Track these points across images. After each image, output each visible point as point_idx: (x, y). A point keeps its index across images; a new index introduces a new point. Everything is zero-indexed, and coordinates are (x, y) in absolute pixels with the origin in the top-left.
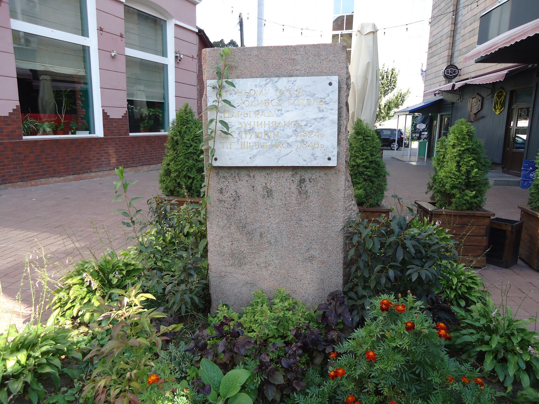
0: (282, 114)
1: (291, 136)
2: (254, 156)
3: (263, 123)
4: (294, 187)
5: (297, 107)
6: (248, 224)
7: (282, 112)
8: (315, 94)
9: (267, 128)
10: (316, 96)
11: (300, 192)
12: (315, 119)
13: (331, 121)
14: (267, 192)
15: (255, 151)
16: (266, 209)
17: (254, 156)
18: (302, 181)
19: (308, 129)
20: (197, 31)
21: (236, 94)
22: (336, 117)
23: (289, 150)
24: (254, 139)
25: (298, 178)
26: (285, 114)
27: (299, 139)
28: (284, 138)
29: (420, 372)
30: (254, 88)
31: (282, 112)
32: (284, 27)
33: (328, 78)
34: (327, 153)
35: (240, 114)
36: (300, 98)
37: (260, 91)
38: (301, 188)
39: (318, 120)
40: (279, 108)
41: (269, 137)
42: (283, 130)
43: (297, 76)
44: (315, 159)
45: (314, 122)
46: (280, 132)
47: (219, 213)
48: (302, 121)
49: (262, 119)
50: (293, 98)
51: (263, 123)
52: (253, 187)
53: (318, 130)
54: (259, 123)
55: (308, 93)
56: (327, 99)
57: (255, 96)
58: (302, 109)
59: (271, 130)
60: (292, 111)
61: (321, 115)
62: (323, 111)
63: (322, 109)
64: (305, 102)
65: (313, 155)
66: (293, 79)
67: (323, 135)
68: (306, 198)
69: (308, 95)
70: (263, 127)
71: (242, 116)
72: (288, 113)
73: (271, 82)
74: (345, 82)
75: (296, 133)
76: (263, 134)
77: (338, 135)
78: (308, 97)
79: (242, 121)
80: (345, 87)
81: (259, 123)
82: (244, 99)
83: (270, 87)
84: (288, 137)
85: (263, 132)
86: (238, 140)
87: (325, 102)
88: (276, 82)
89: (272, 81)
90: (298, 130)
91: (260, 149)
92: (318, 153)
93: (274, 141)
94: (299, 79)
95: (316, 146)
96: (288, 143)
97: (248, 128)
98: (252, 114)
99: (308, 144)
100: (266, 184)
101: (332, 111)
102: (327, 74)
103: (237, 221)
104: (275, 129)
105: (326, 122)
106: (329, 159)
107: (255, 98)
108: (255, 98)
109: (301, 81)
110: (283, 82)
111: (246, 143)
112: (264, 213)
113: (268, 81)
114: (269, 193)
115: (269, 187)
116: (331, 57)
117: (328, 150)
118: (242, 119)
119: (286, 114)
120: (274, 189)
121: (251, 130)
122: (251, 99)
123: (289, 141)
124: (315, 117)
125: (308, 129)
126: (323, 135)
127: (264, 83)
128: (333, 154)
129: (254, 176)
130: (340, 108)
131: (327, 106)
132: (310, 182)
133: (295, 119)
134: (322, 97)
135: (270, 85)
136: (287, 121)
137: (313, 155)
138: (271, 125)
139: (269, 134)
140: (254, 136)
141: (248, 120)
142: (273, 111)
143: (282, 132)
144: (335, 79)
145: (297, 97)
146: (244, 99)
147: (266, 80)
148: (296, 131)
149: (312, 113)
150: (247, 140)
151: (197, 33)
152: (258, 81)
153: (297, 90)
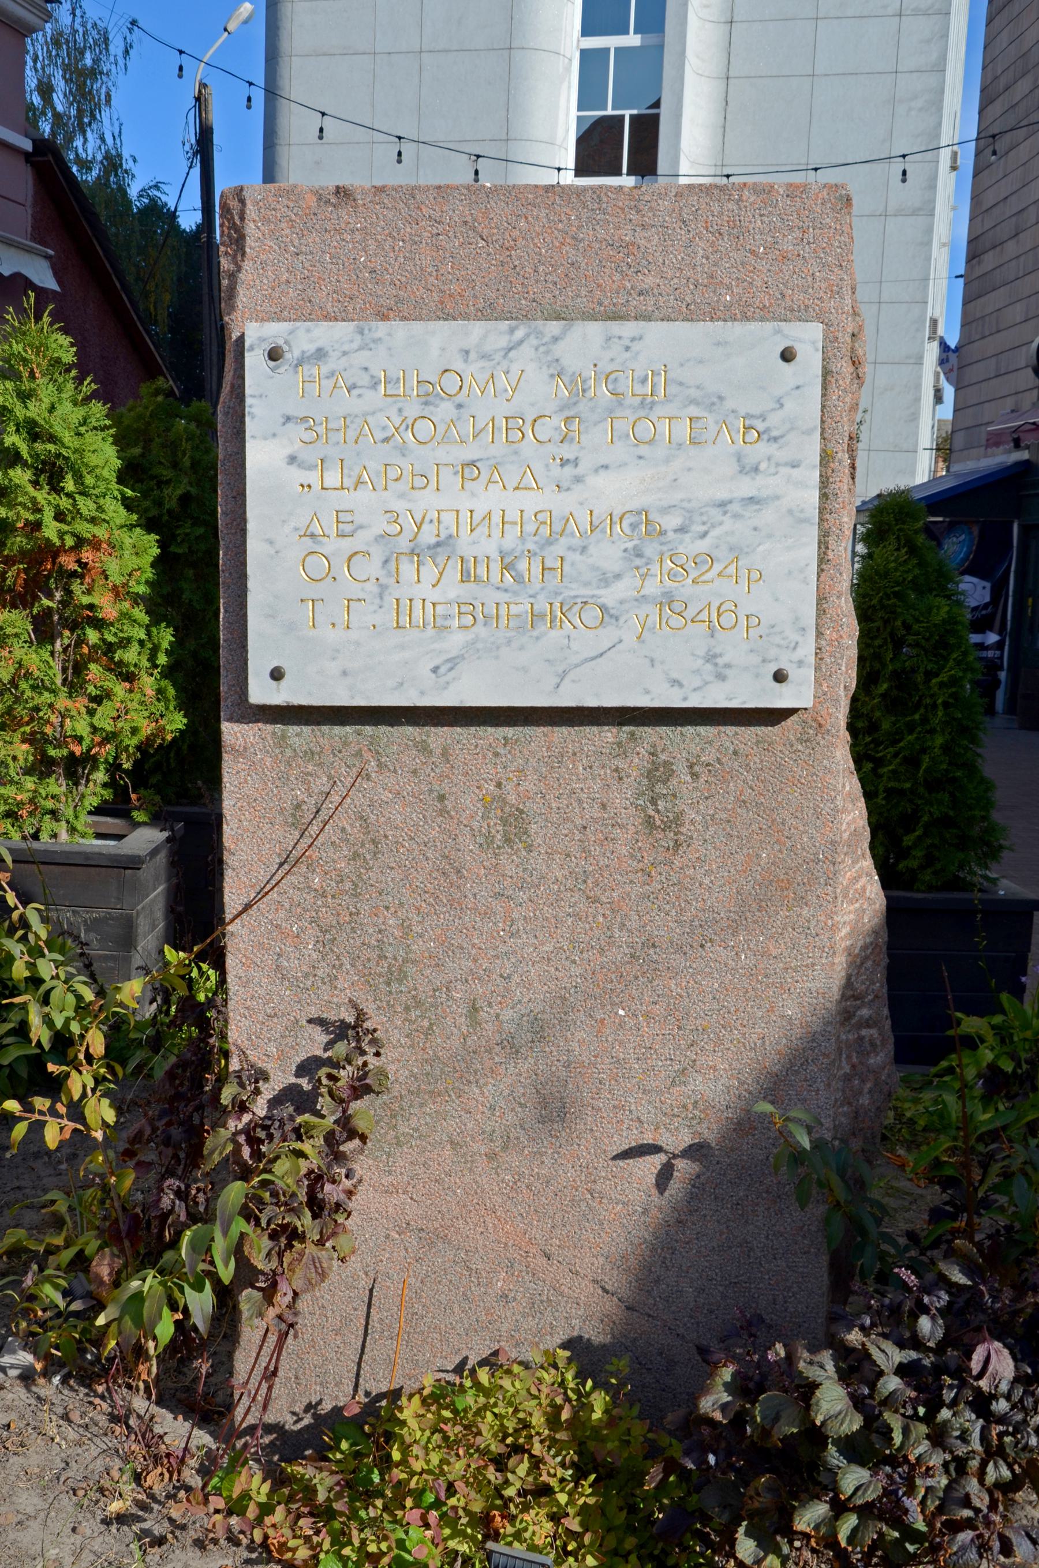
0: (578, 480)
1: (618, 576)
2: (453, 662)
3: (496, 518)
4: (622, 799)
5: (643, 450)
6: (414, 962)
7: (580, 470)
8: (721, 398)
9: (511, 540)
10: (729, 404)
11: (649, 822)
12: (722, 504)
13: (790, 512)
14: (505, 822)
15: (456, 641)
16: (498, 895)
17: (453, 662)
18: (658, 772)
19: (690, 546)
20: (27, 145)
21: (375, 385)
22: (813, 497)
23: (607, 636)
24: (452, 589)
25: (637, 762)
26: (592, 480)
27: (652, 588)
28: (587, 584)
29: (108, 1325)
30: (458, 365)
31: (580, 470)
32: (407, 149)
33: (778, 332)
34: (773, 653)
35: (394, 473)
36: (659, 411)
37: (482, 377)
38: (654, 802)
39: (735, 507)
40: (568, 452)
41: (518, 579)
42: (584, 549)
43: (647, 318)
44: (721, 677)
45: (715, 513)
46: (570, 557)
47: (282, 914)
48: (666, 510)
49: (489, 499)
50: (628, 412)
51: (496, 518)
52: (442, 798)
53: (737, 552)
54: (477, 517)
55: (693, 392)
56: (774, 420)
57: (461, 398)
58: (667, 461)
59: (531, 546)
60: (623, 465)
61: (746, 487)
62: (756, 469)
63: (750, 461)
64: (683, 430)
65: (711, 657)
66: (629, 329)
67: (756, 575)
68: (677, 844)
69: (693, 402)
70: (497, 533)
71: (403, 486)
72: (602, 472)
73: (533, 341)
74: (845, 350)
75: (638, 562)
76: (496, 567)
77: (820, 571)
78: (694, 411)
79: (399, 506)
80: (847, 368)
81: (477, 517)
82: (412, 410)
83: (525, 358)
84: (606, 580)
85: (495, 555)
86: (383, 588)
87: (767, 430)
88: (556, 339)
89: (540, 334)
90: (651, 550)
91: (480, 629)
92: (734, 648)
93: (541, 597)
94: (655, 331)
95: (728, 619)
96: (603, 608)
97: (428, 536)
98: (450, 480)
99: (690, 613)
100: (499, 785)
101: (795, 472)
102: (765, 314)
103: (368, 953)
104: (549, 542)
105: (768, 516)
106: (779, 677)
107: (459, 406)
108: (459, 406)
109: (662, 342)
110: (585, 343)
111: (418, 605)
112: (487, 914)
113: (519, 334)
114: (515, 826)
115: (512, 799)
116: (787, 244)
117: (777, 640)
118: (402, 496)
119: (600, 481)
120: (531, 807)
121: (443, 544)
122: (445, 410)
123: (610, 596)
124: (723, 495)
125: (690, 546)
126: (756, 575)
127: (503, 342)
128: (800, 653)
129: (445, 753)
130: (826, 458)
131: (772, 449)
132: (695, 776)
133: (634, 504)
134: (755, 411)
135: (526, 351)
136: (601, 511)
137: (711, 657)
138: (530, 528)
139: (522, 565)
140: (454, 572)
141: (427, 501)
142: (538, 467)
143: (577, 557)
144: (808, 337)
145: (647, 404)
146: (412, 410)
147: (512, 331)
148: (639, 555)
149: (709, 476)
150: (425, 590)
151: (27, 156)
152: (476, 332)
153: (644, 381)
